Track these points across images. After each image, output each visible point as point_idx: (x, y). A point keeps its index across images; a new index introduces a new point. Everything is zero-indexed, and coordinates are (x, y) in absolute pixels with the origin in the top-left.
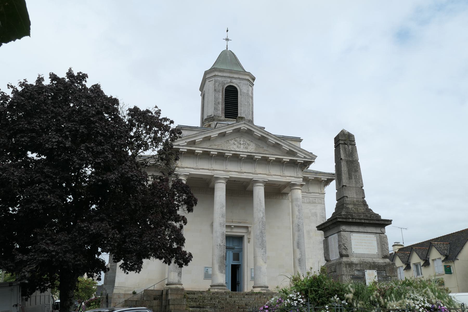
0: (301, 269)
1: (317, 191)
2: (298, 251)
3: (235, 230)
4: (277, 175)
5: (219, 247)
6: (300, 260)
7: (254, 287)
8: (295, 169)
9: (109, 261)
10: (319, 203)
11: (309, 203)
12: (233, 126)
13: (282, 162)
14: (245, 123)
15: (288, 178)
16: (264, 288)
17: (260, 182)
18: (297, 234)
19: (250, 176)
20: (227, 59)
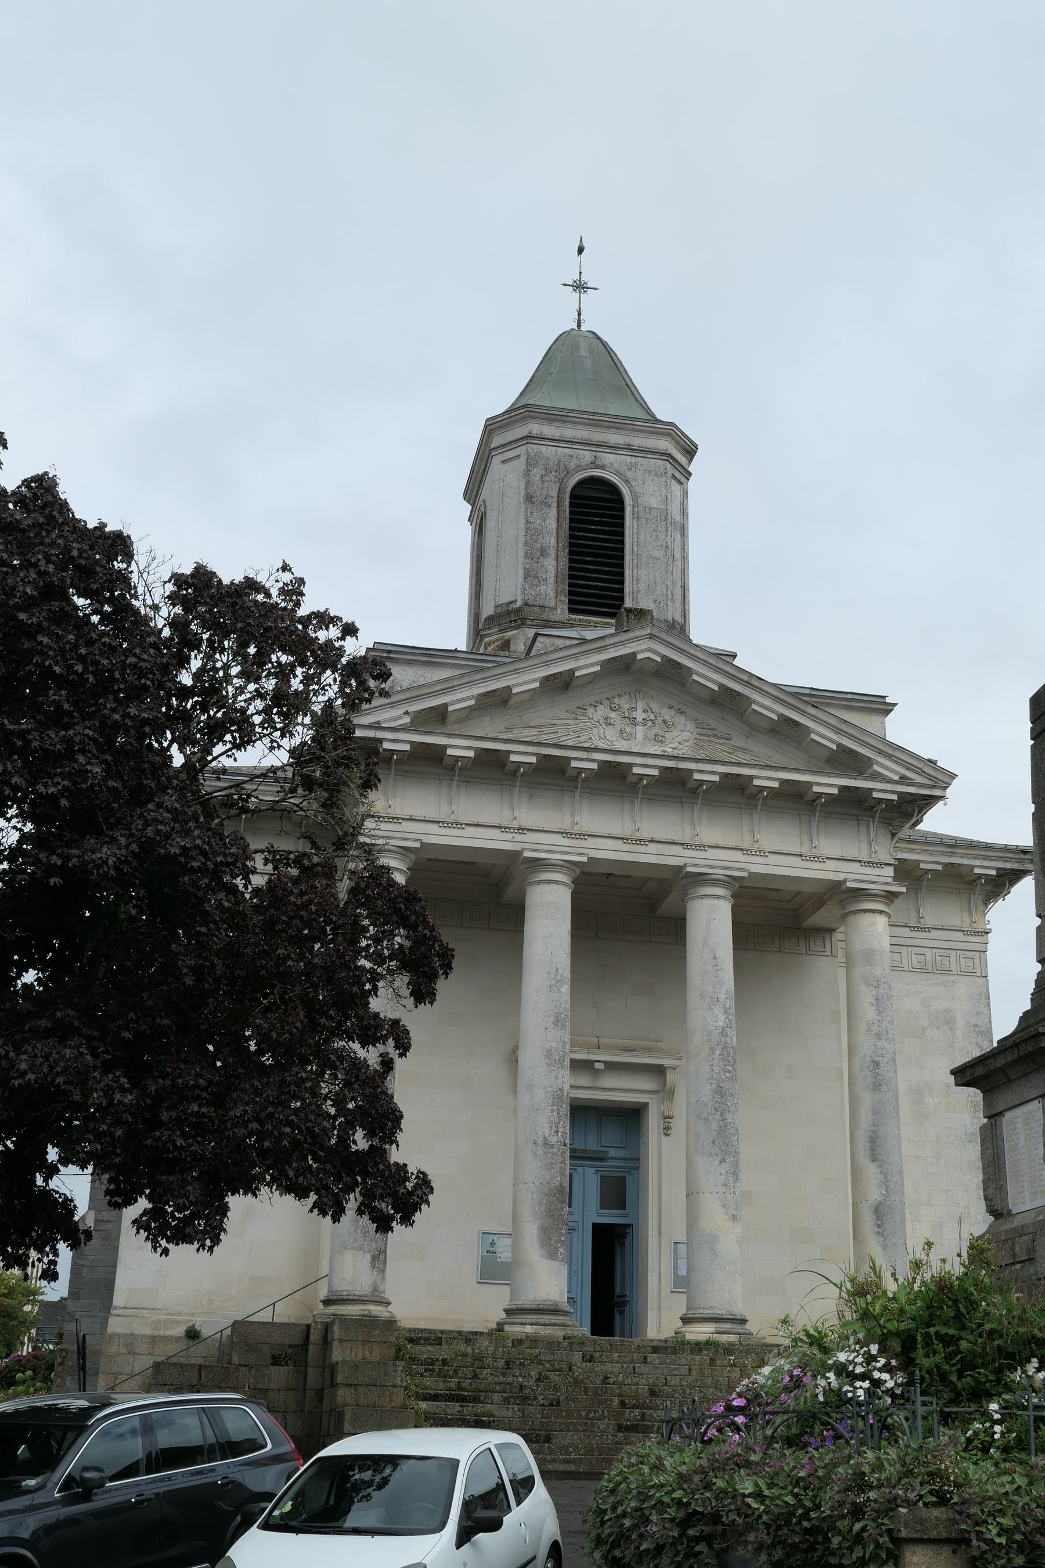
2: (871, 1172)
3: (610, 1081)
5: (540, 1151)
6: (879, 1211)
7: (686, 1320)
11: (922, 970)
12: (605, 648)
14: (651, 637)
15: (831, 865)
16: (727, 1326)
18: (867, 1099)
19: (674, 857)
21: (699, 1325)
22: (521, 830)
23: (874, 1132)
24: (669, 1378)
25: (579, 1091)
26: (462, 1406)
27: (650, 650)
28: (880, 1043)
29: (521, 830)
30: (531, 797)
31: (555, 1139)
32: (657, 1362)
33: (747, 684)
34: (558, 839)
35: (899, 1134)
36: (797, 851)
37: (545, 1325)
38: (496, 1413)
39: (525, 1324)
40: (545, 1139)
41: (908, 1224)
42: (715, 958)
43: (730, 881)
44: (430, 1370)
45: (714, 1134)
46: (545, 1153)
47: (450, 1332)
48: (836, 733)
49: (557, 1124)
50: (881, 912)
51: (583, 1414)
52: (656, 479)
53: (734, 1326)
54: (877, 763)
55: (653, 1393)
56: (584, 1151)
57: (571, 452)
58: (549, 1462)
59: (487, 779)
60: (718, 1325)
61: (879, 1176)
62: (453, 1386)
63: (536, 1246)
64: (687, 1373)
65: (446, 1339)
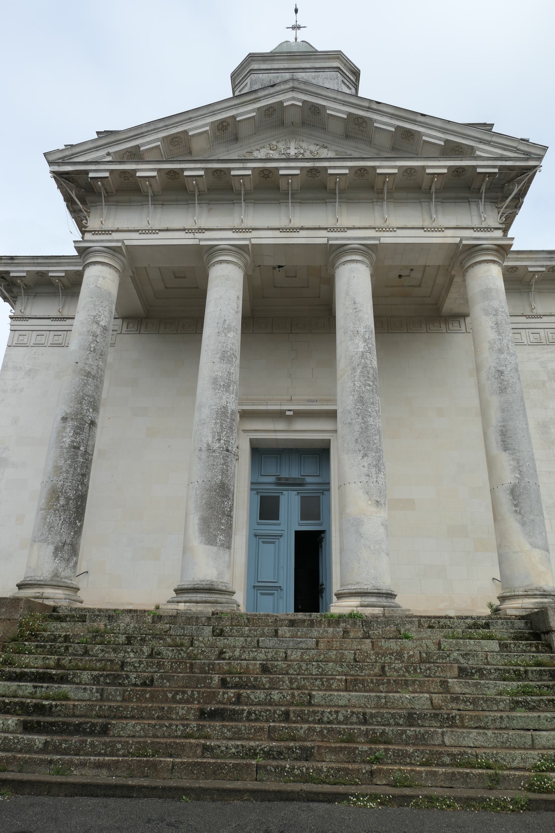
0: (523, 524)
2: (504, 460)
3: (300, 425)
4: (411, 228)
5: (204, 455)
6: (514, 492)
8: (474, 207)
11: (539, 343)
12: (258, 100)
13: (425, 185)
15: (449, 233)
16: (372, 600)
17: (354, 251)
18: (495, 401)
19: (320, 238)
21: (347, 600)
22: (201, 230)
23: (504, 426)
24: (289, 652)
25: (277, 434)
26: (35, 687)
27: (293, 99)
28: (502, 356)
29: (201, 230)
30: (210, 210)
31: (218, 445)
32: (288, 635)
33: (369, 109)
34: (230, 234)
35: (527, 428)
36: (420, 224)
37: (197, 602)
38: (71, 695)
39: (178, 602)
40: (208, 445)
41: (547, 522)
42: (355, 303)
44: (41, 647)
45: (357, 434)
46: (208, 457)
47: (107, 610)
48: (443, 133)
49: (219, 434)
50: (494, 262)
51: (170, 695)
52: (331, 81)
53: (380, 599)
54: (479, 149)
55: (265, 669)
56: (287, 479)
57: (278, 75)
58: (76, 766)
59: (177, 201)
60: (363, 599)
61: (512, 463)
62: (52, 663)
63: (197, 533)
64: (314, 646)
65: (90, 616)
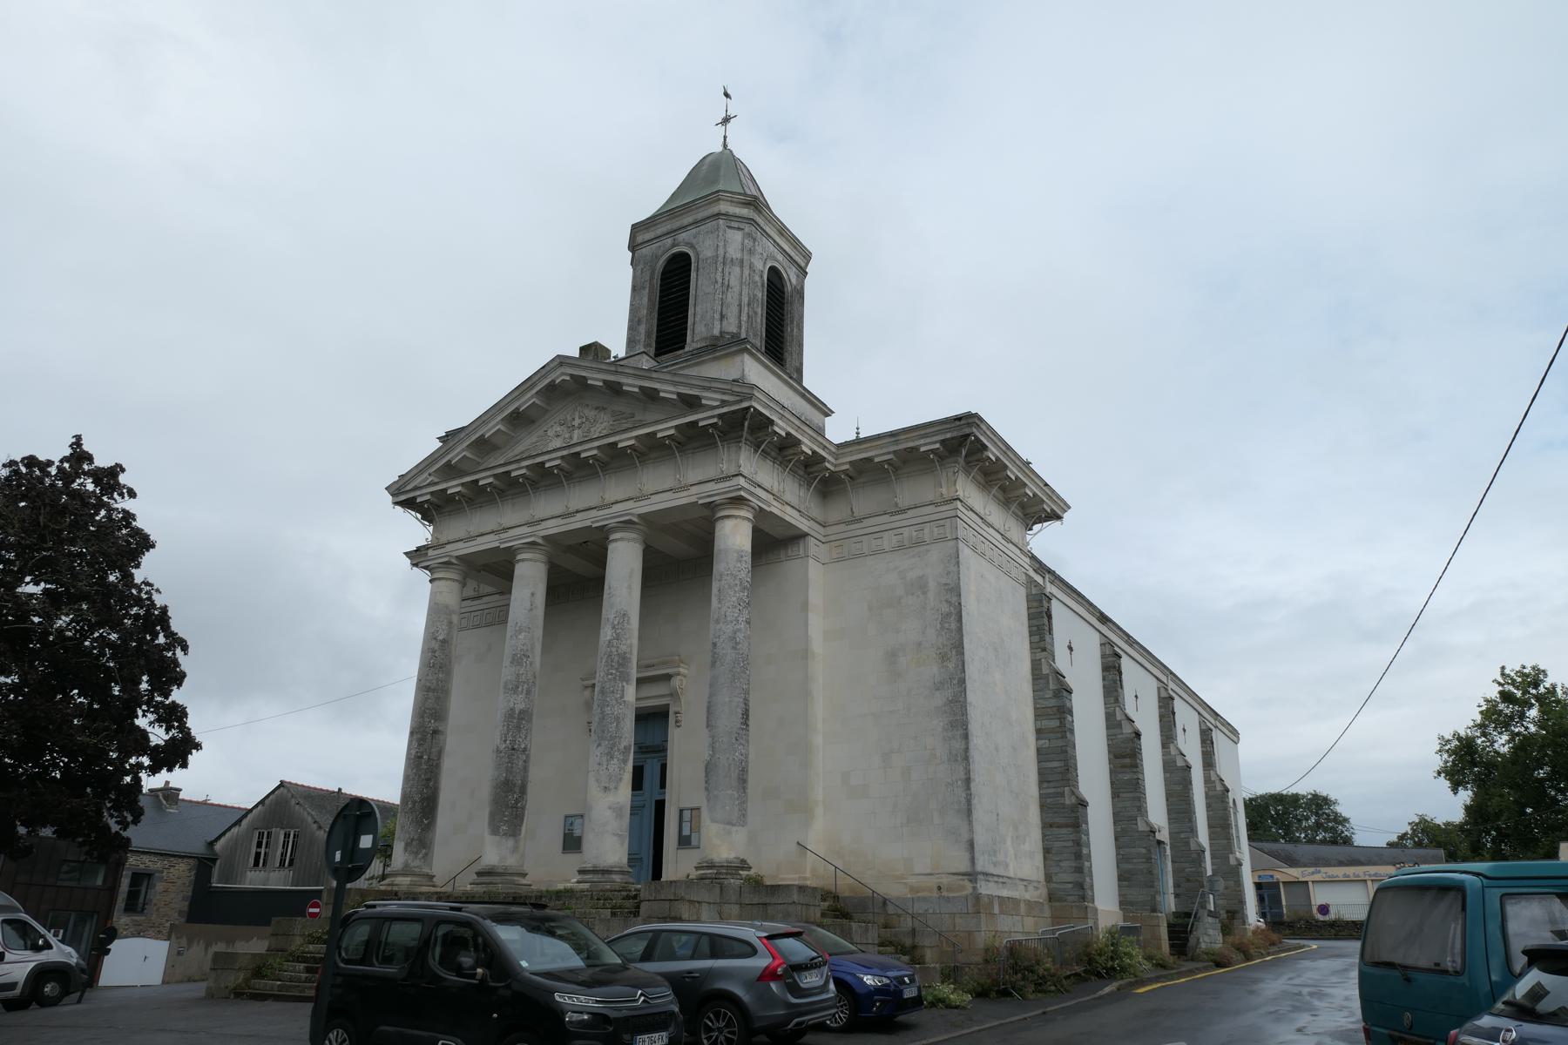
1: (930, 497)
4: (663, 489)
9: (1169, 812)
10: (937, 540)
11: (901, 547)
20: (720, 190)
33: (545, 376)
43: (761, 514)
